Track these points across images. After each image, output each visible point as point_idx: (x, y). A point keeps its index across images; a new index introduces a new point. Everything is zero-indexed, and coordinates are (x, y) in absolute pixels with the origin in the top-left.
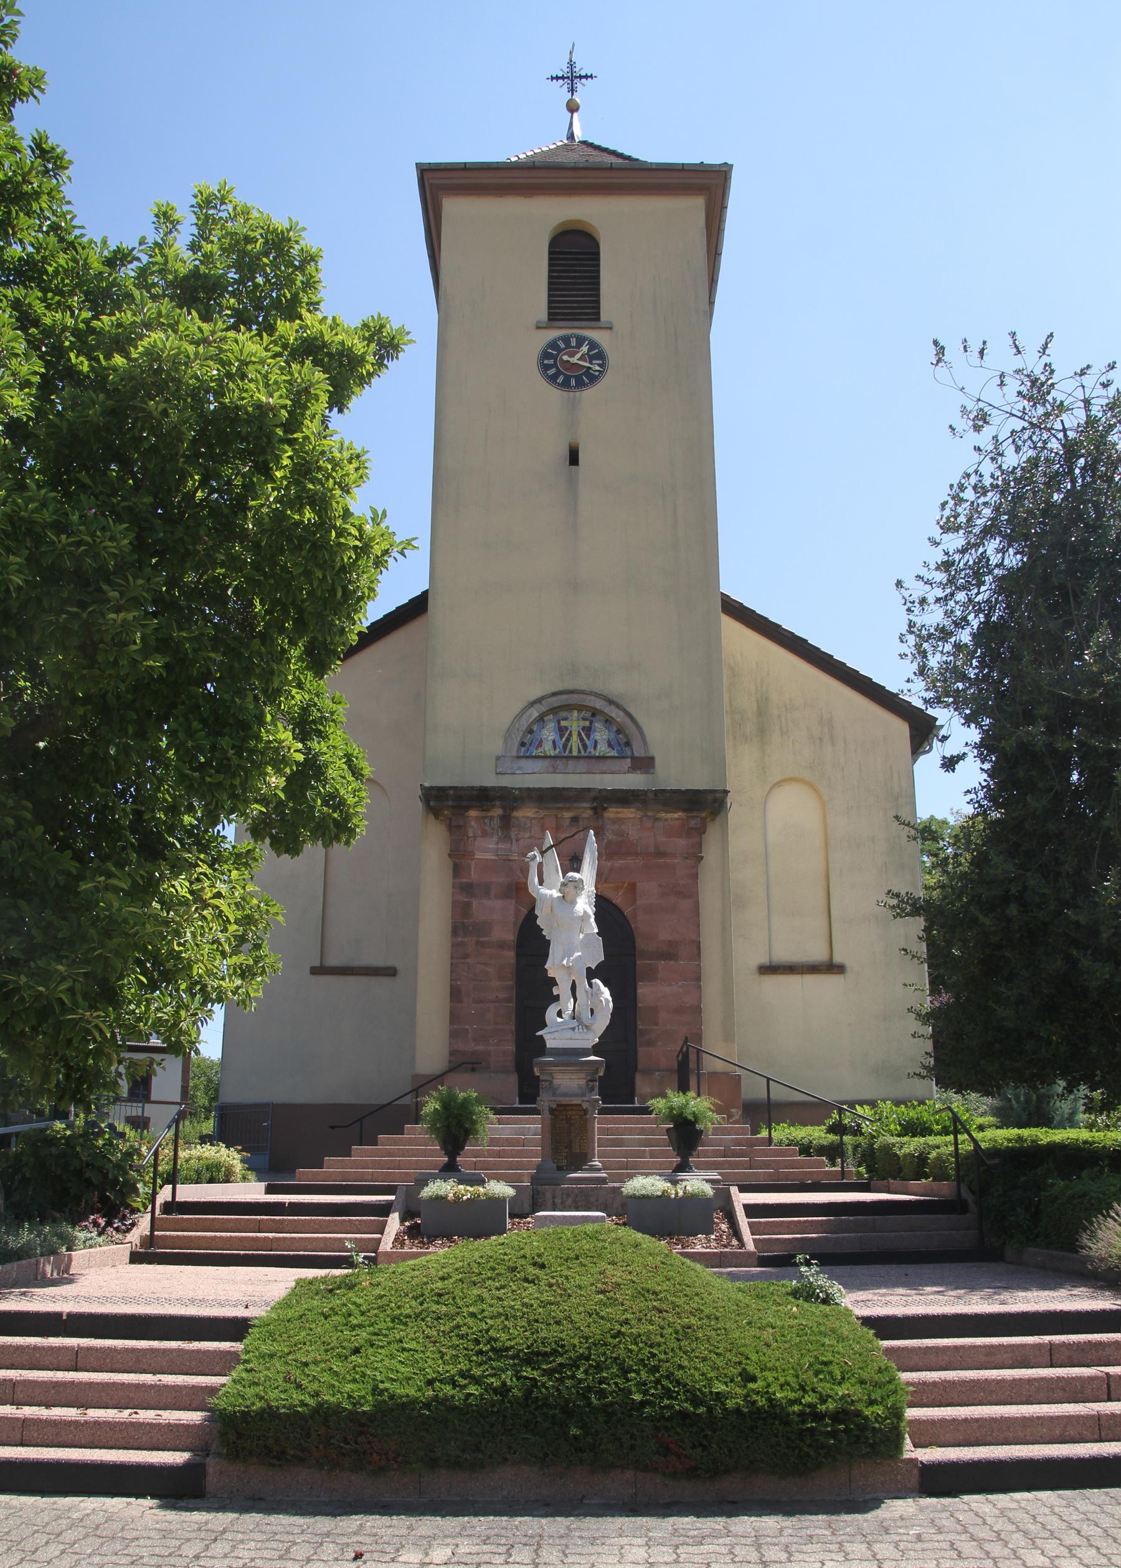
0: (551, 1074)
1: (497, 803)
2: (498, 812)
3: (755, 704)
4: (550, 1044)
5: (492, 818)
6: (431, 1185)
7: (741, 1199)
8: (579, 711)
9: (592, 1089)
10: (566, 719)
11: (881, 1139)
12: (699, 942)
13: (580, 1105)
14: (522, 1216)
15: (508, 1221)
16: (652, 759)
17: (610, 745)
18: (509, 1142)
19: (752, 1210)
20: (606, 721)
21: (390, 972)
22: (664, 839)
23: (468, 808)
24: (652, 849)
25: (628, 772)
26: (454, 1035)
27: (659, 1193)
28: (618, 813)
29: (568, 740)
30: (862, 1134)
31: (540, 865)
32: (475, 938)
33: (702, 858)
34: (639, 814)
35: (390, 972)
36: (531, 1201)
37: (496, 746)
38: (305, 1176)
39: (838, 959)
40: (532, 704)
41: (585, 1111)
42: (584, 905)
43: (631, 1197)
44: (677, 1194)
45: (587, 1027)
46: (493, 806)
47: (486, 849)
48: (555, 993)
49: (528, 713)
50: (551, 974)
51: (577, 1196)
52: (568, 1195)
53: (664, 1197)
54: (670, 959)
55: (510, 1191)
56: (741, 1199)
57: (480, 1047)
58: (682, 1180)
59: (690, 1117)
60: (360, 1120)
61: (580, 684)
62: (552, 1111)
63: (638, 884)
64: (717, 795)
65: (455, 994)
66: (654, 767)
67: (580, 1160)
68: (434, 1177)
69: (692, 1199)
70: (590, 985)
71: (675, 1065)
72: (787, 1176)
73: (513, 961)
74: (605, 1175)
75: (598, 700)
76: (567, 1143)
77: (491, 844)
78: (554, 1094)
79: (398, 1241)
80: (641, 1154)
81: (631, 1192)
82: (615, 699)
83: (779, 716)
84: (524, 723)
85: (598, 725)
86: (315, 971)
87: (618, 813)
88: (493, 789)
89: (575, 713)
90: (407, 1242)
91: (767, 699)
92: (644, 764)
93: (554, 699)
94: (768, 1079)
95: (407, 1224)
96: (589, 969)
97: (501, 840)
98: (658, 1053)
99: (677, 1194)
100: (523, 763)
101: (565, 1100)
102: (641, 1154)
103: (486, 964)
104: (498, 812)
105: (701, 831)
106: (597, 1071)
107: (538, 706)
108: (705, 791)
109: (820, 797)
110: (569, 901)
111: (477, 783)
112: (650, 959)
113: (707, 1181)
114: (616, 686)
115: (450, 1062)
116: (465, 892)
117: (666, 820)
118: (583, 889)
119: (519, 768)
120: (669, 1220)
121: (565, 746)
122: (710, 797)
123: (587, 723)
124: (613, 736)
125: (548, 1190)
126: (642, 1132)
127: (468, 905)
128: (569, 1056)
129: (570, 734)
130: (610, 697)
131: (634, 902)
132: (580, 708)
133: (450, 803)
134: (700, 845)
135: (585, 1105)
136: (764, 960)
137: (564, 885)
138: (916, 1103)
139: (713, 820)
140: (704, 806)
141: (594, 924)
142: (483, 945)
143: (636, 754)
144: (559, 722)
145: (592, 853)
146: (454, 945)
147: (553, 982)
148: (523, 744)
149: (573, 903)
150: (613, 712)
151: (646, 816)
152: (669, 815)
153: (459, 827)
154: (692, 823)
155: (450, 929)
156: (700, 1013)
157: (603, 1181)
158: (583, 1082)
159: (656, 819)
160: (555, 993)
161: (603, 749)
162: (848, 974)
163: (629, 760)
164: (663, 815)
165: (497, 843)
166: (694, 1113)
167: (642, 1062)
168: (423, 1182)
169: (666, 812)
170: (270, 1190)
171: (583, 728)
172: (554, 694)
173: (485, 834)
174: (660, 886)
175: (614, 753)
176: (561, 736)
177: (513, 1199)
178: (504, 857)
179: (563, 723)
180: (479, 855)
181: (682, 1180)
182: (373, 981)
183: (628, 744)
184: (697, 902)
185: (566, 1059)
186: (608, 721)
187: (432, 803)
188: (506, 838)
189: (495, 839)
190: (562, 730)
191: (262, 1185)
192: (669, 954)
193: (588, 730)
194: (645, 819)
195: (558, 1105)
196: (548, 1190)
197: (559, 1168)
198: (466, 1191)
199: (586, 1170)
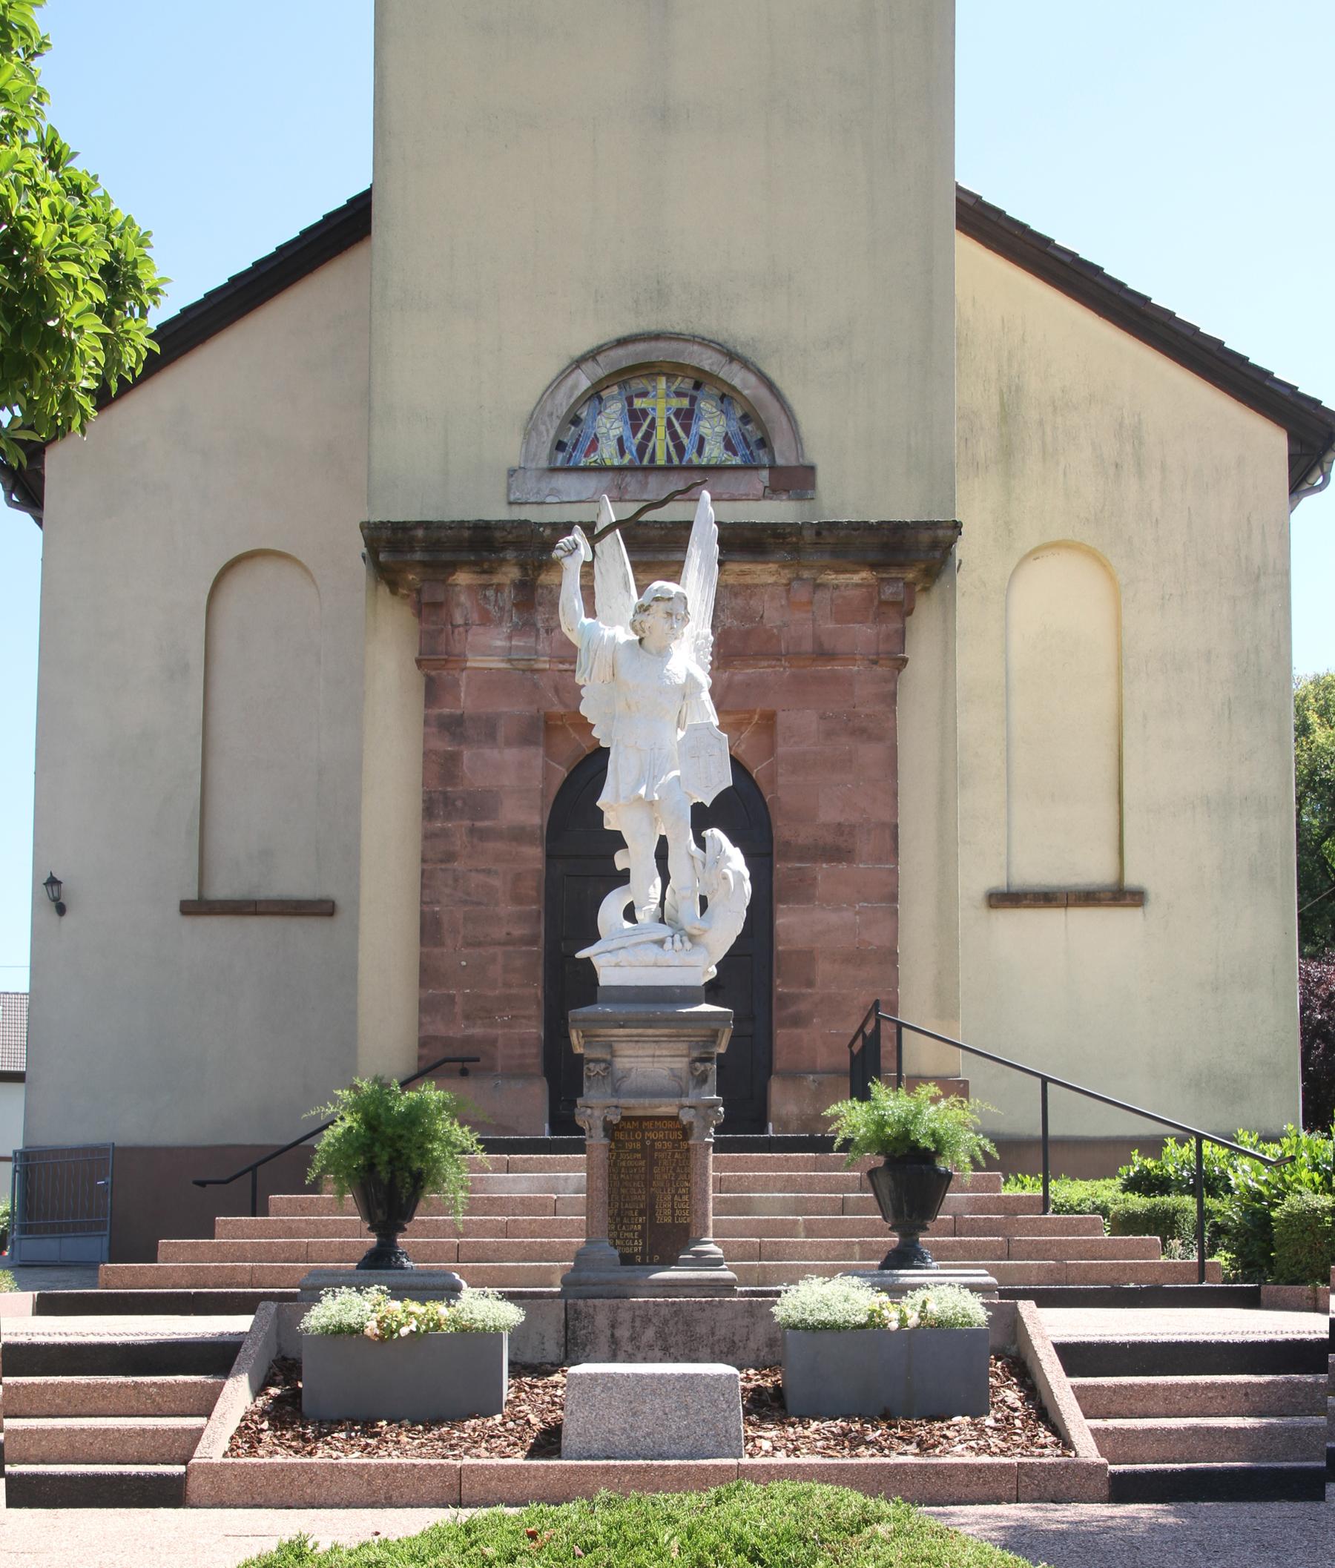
0: (610, 1046)
1: (510, 555)
2: (510, 574)
3: (995, 400)
4: (608, 976)
5: (499, 588)
6: (327, 1300)
7: (1050, 1327)
8: (670, 377)
9: (703, 1079)
10: (644, 394)
11: (1292, 1199)
12: (896, 826)
13: (675, 1118)
14: (541, 1370)
15: (506, 1381)
16: (811, 469)
17: (729, 446)
18: (526, 1206)
19: (1078, 1357)
20: (723, 397)
21: (323, 909)
22: (831, 626)
23: (453, 567)
24: (807, 646)
25: (764, 497)
26: (426, 1007)
27: (862, 1318)
28: (743, 573)
29: (648, 436)
30: (1229, 1190)
31: (588, 567)
32: (467, 823)
33: (905, 661)
34: (787, 574)
35: (323, 909)
36: (568, 1327)
37: (510, 449)
38: (120, 1276)
39: (1133, 879)
40: (578, 363)
41: (686, 1131)
42: (689, 656)
43: (794, 1327)
44: (903, 1320)
45: (692, 938)
46: (503, 561)
47: (488, 649)
48: (619, 867)
49: (570, 381)
50: (611, 823)
51: (666, 1322)
52: (647, 1321)
53: (872, 1327)
54: (839, 860)
55: (511, 1314)
56: (1050, 1327)
57: (477, 1031)
58: (915, 1287)
59: (926, 1143)
60: (253, 1169)
61: (672, 320)
62: (610, 1129)
63: (781, 716)
64: (940, 533)
65: (430, 929)
66: (813, 486)
67: (671, 1240)
68: (336, 1281)
69: (939, 1332)
70: (701, 842)
71: (845, 1061)
72: (1085, 1274)
73: (540, 865)
74: (729, 1275)
75: (709, 353)
76: (646, 1216)
77: (498, 638)
78: (616, 1092)
79: (247, 1436)
80: (789, 1230)
81: (796, 1316)
82: (739, 350)
83: (1041, 423)
84: (562, 402)
85: (707, 406)
86: (192, 908)
87: (743, 573)
88: (501, 525)
89: (662, 383)
90: (266, 1436)
91: (1018, 389)
92: (797, 480)
93: (621, 352)
94: (1045, 1080)
95: (274, 1391)
96: (698, 809)
97: (517, 631)
98: (818, 1038)
99: (903, 1320)
100: (562, 481)
101: (642, 1107)
102: (789, 1230)
103: (488, 872)
104: (510, 574)
105: (905, 609)
106: (714, 1038)
107: (589, 366)
108: (917, 526)
109: (1112, 578)
110: (652, 667)
111: (472, 515)
112: (801, 859)
113: (973, 1288)
114: (742, 325)
115: (420, 1058)
116: (449, 730)
117: (837, 587)
118: (685, 619)
119: (554, 492)
120: (897, 1385)
121: (641, 449)
122: (925, 537)
123: (685, 403)
124: (735, 426)
125: (601, 1311)
126: (789, 1185)
127: (453, 758)
128: (654, 1004)
129: (652, 425)
130: (730, 346)
131: (771, 750)
132: (673, 370)
133: (418, 556)
134: (902, 635)
135: (686, 1116)
136: (997, 881)
137: (643, 609)
139: (926, 590)
140: (911, 556)
141: (710, 706)
142: (484, 835)
143: (780, 461)
144: (631, 404)
146: (428, 837)
147: (617, 841)
148: (560, 446)
149: (663, 653)
150: (738, 378)
151: (799, 578)
152: (842, 578)
153: (436, 606)
154: (888, 592)
155: (418, 805)
156: (895, 962)
157: (727, 1287)
158: (681, 1064)
159: (818, 587)
160: (619, 867)
161: (714, 452)
162: (1152, 906)
163: (765, 474)
164: (831, 578)
165: (510, 638)
166: (934, 1134)
167: (781, 1059)
168: (311, 1295)
169: (837, 572)
170: (46, 1306)
171: (678, 413)
172: (622, 342)
173: (486, 620)
174: (823, 717)
175: (737, 461)
176: (635, 429)
177: (518, 1334)
178: (521, 665)
179: (639, 403)
180: (474, 662)
181: (915, 1287)
182: (295, 927)
183: (763, 443)
184: (893, 750)
185: (642, 1010)
186: (727, 397)
187: (382, 557)
188: (527, 627)
189: (506, 629)
190: (636, 417)
191: (28, 1298)
192: (837, 850)
193: (687, 416)
194: (795, 585)
195: (624, 1118)
196: (601, 1311)
197: (627, 1260)
198: (409, 1315)
199: (686, 1263)
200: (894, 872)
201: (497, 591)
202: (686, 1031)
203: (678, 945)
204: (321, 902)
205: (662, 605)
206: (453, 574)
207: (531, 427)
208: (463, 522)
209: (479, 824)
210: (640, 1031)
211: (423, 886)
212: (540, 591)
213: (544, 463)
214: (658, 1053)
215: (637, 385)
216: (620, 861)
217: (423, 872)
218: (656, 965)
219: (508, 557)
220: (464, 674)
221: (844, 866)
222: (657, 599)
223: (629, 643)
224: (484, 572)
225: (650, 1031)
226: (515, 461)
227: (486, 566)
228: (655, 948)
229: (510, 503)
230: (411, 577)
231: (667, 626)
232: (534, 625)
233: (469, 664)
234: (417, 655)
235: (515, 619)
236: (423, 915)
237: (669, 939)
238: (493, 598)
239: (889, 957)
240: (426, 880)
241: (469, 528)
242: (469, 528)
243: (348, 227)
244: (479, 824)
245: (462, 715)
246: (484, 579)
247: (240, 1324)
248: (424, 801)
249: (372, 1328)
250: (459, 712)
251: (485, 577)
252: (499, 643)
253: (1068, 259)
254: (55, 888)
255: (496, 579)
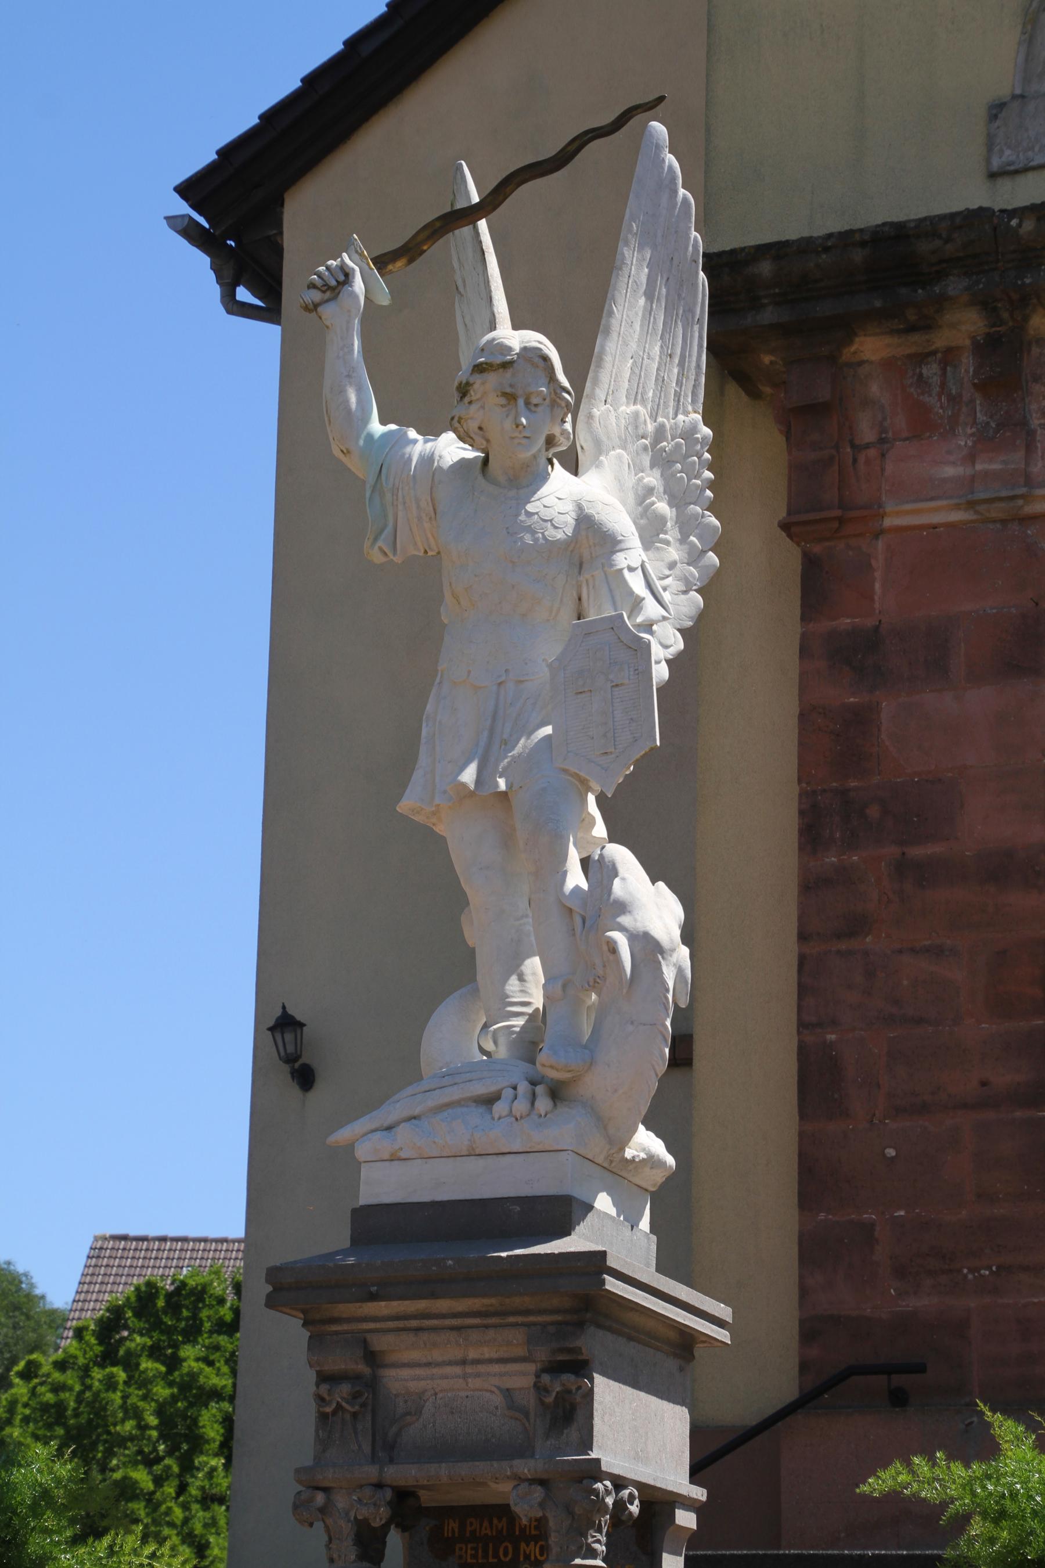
1: (955, 286)
2: (963, 326)
5: (949, 357)
23: (847, 327)
26: (815, 1251)
57: (924, 1302)
97: (986, 441)
104: (963, 326)
115: (804, 1366)
127: (859, 721)
133: (768, 316)
135: (526, 1506)
138: (188, 1421)
145: (666, 268)
146: (810, 886)
158: (521, 1378)
165: (971, 458)
173: (922, 425)
180: (899, 515)
188: (1012, 430)
189: (963, 441)
201: (944, 364)
202: (517, 1301)
203: (521, 1106)
205: (492, 379)
206: (851, 342)
208: (850, 233)
209: (917, 852)
210: (421, 1305)
211: (803, 990)
212: (1035, 350)
214: (472, 1354)
218: (472, 1154)
219: (951, 292)
220: (880, 544)
222: (479, 369)
223: (462, 465)
224: (912, 329)
225: (443, 1305)
227: (912, 316)
228: (475, 1115)
229: (993, 176)
230: (767, 359)
231: (508, 424)
232: (1024, 423)
233: (888, 522)
234: (783, 514)
235: (981, 417)
236: (803, 1053)
237: (508, 1093)
238: (936, 380)
240: (810, 976)
241: (863, 244)
242: (863, 244)
244: (917, 852)
245: (876, 629)
246: (914, 343)
248: (802, 813)
250: (870, 622)
251: (916, 337)
252: (950, 471)
254: (289, 1037)
255: (941, 340)
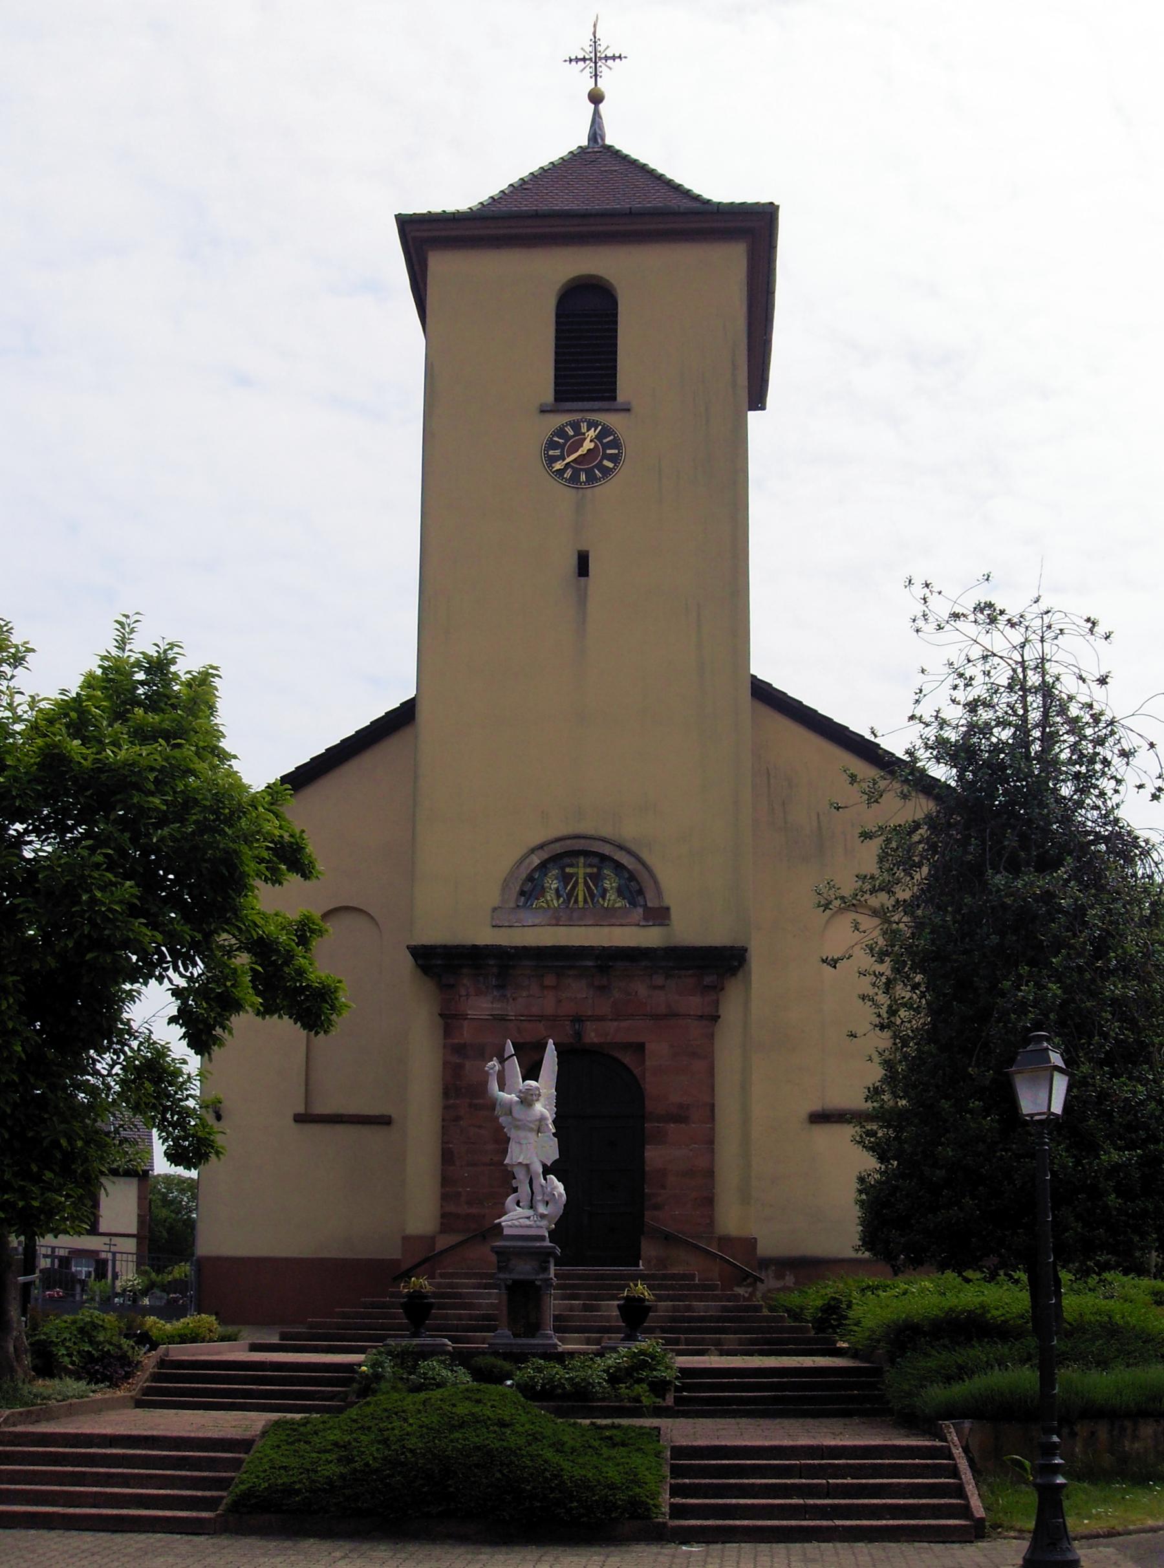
10: (571, 866)
12: (713, 1105)
16: (668, 909)
26: (445, 1197)
35: (385, 1121)
37: (492, 895)
40: (533, 851)
42: (544, 1108)
49: (527, 861)
65: (447, 1157)
86: (299, 1119)
92: (659, 915)
93: (557, 845)
103: (480, 1127)
114: (629, 831)
123: (595, 870)
127: (461, 1066)
129: (576, 882)
136: (816, 1107)
150: (625, 859)
192: (680, 1116)
200: (713, 1129)
204: (382, 1116)
207: (505, 886)
209: (476, 1101)
211: (443, 1134)
213: (512, 905)
215: (567, 860)
216: (514, 1183)
217: (443, 1127)
221: (683, 1126)
226: (496, 903)
239: (710, 1174)
243: (400, 719)
244: (476, 1101)
247: (360, 1357)
249: (299, 1024)
253: (858, 739)
